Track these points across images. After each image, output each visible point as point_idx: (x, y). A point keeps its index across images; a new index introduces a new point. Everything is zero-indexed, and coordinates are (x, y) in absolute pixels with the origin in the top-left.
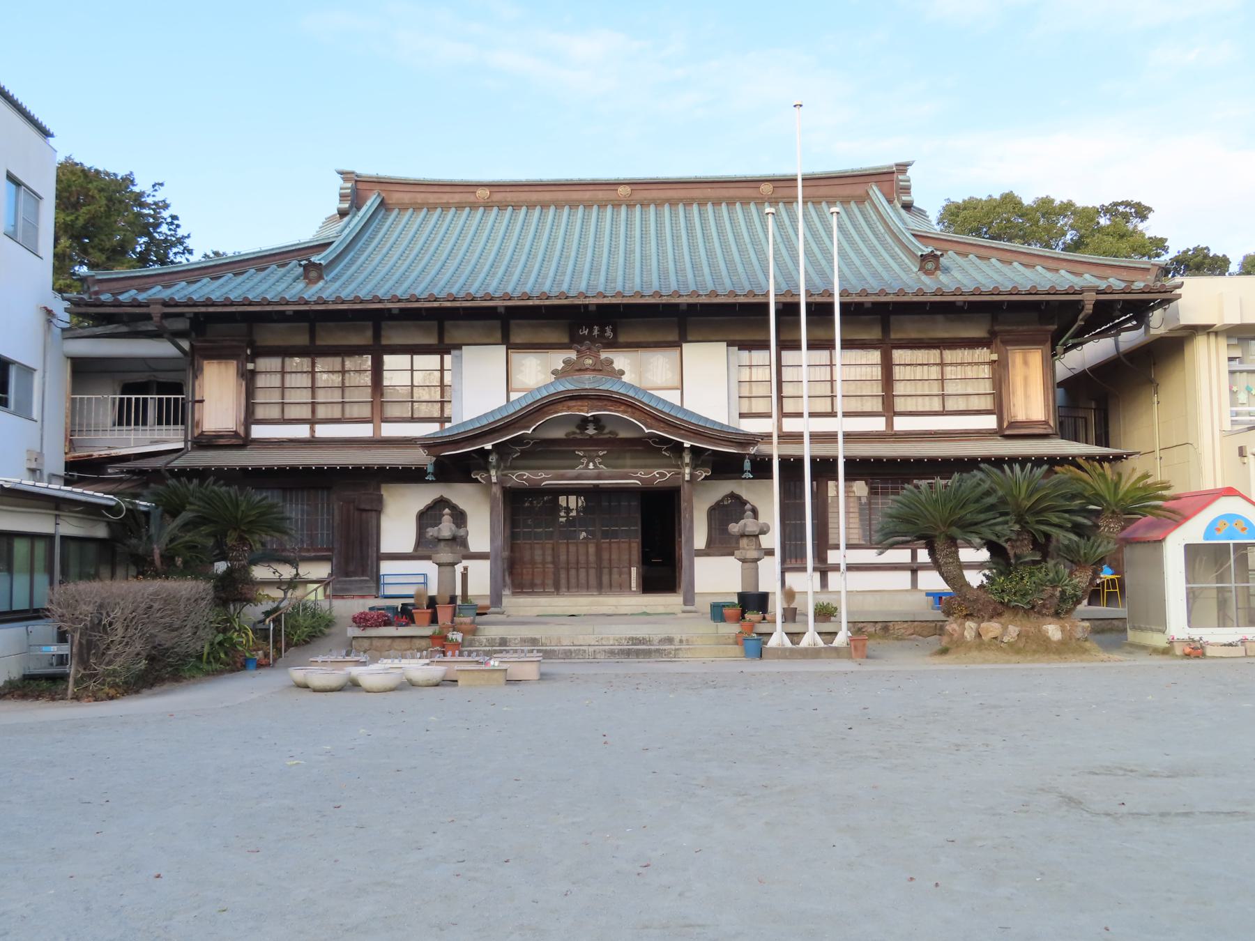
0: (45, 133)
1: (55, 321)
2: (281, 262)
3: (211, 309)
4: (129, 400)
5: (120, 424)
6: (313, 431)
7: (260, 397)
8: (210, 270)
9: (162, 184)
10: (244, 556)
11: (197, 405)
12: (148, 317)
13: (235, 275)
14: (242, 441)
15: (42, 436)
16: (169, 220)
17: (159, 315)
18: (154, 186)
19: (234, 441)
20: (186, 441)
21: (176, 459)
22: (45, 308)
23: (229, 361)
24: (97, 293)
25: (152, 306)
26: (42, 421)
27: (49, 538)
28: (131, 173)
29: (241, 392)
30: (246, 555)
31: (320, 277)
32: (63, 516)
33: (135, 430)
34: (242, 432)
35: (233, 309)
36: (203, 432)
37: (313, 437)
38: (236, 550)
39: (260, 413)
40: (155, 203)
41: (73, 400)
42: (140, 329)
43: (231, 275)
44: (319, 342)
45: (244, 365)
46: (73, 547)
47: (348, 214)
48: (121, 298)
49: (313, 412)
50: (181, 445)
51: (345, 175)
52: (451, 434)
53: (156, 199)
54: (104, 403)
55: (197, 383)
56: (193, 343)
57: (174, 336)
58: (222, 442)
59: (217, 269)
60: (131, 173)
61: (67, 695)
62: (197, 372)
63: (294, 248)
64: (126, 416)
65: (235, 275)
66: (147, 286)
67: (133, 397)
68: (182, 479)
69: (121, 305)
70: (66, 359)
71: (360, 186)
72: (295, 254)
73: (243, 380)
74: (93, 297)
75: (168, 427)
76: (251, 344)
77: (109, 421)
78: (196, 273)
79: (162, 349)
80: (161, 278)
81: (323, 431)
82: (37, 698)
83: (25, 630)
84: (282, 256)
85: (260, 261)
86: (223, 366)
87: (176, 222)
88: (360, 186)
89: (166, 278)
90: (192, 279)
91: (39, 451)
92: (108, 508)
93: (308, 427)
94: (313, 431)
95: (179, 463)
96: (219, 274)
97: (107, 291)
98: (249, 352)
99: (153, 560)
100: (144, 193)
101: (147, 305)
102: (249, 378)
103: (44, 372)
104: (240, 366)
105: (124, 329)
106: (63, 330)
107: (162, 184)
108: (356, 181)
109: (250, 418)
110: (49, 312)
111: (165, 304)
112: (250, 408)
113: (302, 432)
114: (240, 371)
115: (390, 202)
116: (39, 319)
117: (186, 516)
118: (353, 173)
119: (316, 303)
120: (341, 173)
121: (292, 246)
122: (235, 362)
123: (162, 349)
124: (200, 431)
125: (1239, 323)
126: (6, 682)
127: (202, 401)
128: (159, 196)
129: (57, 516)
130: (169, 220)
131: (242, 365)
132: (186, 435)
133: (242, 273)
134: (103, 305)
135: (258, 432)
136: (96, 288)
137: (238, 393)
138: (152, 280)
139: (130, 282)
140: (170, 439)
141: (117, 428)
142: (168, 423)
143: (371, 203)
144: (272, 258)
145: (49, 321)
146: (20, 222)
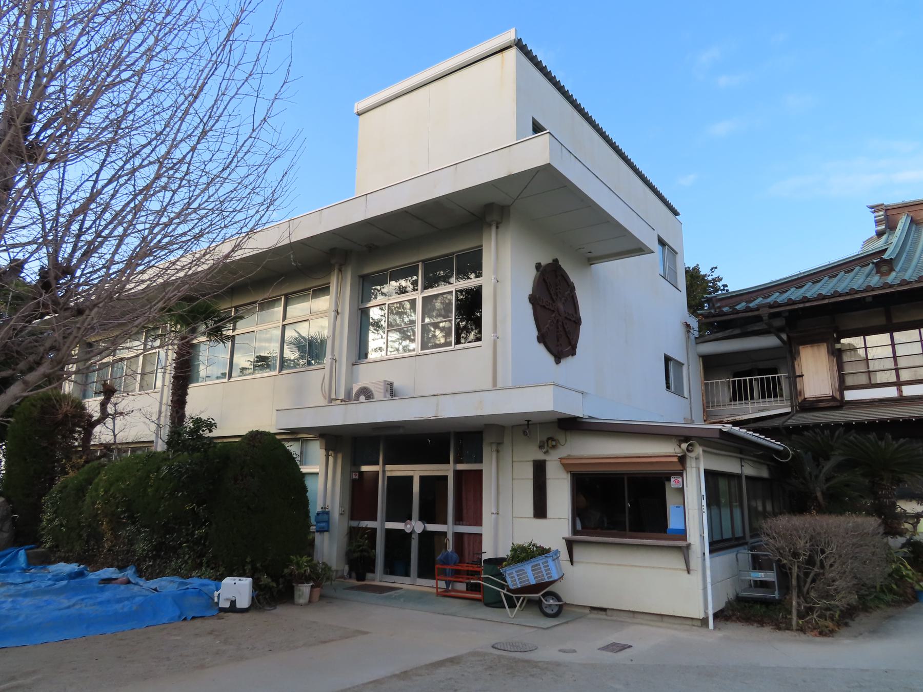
0: (676, 213)
1: (691, 331)
2: (847, 269)
3: (808, 305)
4: (745, 381)
5: (735, 400)
6: (900, 391)
7: (848, 369)
8: (794, 283)
9: (716, 268)
10: (894, 494)
11: (798, 379)
12: (759, 319)
13: (813, 283)
14: (838, 403)
15: (691, 408)
16: (722, 288)
17: (767, 315)
18: (711, 269)
19: (831, 404)
20: (792, 406)
21: (788, 419)
22: (686, 323)
23: (820, 344)
24: (719, 307)
25: (761, 310)
26: (690, 398)
27: (738, 477)
28: (698, 265)
29: (833, 366)
30: (895, 493)
31: (892, 270)
32: (746, 459)
33: (745, 403)
34: (838, 396)
35: (826, 301)
36: (805, 399)
37: (901, 396)
38: (885, 489)
39: (849, 381)
40: (713, 279)
41: (706, 384)
42: (749, 330)
43: (810, 283)
44: (895, 321)
45: (833, 346)
46: (723, 484)
47: (885, 233)
48: (738, 307)
49: (898, 376)
50: (788, 410)
51: (875, 208)
52: (13, 582)
53: (713, 277)
54: (723, 387)
55: (796, 363)
56: (789, 334)
57: (777, 332)
58: (822, 405)
59: (799, 281)
60: (698, 265)
61: (791, 625)
62: (793, 356)
63: (855, 258)
64: (740, 394)
65: (813, 283)
66: (752, 299)
67: (748, 378)
68: (825, 431)
69: (738, 312)
70: (698, 357)
71: (890, 213)
72: (856, 262)
73: (834, 356)
74: (717, 310)
75: (770, 400)
76: (836, 330)
77: (727, 400)
78: (784, 286)
79: (770, 341)
80: (761, 292)
81: (908, 391)
82: (761, 623)
83: (735, 556)
84: (847, 265)
85: (831, 271)
86: (816, 348)
87: (726, 288)
88: (890, 213)
89: (765, 291)
90: (783, 290)
91: (690, 418)
92: (777, 452)
93: (895, 388)
94: (900, 391)
95: (791, 422)
96: (802, 284)
97: (726, 306)
98: (835, 335)
99: (816, 497)
100: (706, 275)
101: (757, 309)
102: (837, 355)
103: (689, 366)
104: (830, 346)
105: (737, 331)
106: (696, 338)
107: (716, 268)
108: (886, 210)
109: (843, 386)
110: (688, 326)
111: (771, 306)
112: (842, 378)
113: (892, 392)
114: (830, 349)
115: (919, 218)
116: (680, 331)
117: (837, 458)
118: (883, 205)
119: (899, 285)
120: (871, 207)
121: (853, 256)
122: (825, 345)
123: (770, 341)
124: (803, 398)
125: (532, 481)
126: (726, 602)
127: (802, 376)
128: (715, 275)
129: (741, 459)
130: (722, 288)
131: (832, 346)
132: (792, 403)
133: (819, 281)
134: (725, 314)
135: (850, 395)
136: (719, 305)
137: (831, 368)
138: (754, 295)
139: (741, 298)
140: (777, 407)
141: (732, 403)
142: (769, 397)
143: (903, 222)
144: (839, 268)
145: (688, 332)
146: (667, 268)
